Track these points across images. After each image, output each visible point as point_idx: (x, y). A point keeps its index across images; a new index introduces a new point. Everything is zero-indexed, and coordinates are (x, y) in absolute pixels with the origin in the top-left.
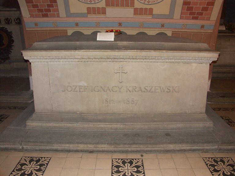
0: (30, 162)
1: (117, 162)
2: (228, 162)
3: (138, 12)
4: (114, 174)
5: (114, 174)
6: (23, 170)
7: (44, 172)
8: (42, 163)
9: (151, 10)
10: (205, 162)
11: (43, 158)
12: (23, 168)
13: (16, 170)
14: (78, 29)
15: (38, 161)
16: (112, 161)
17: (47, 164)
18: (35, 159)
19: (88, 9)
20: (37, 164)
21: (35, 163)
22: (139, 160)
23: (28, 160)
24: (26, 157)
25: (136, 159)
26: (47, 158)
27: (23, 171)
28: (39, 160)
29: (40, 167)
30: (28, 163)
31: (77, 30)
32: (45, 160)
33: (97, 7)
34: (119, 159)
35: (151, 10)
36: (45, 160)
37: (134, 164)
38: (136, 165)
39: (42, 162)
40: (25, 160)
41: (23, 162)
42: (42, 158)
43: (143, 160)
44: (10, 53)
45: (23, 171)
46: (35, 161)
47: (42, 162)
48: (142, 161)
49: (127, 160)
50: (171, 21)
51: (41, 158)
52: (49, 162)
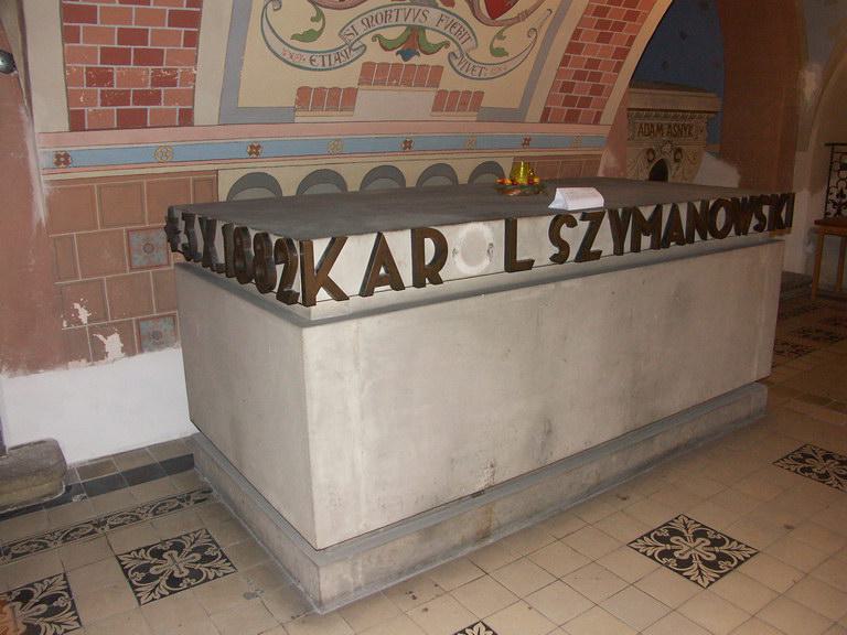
0: (697, 534)
1: (59, 624)
2: (159, 584)
3: (445, 102)
4: (65, 590)
5: (65, 590)
6: (672, 544)
7: (722, 575)
8: (659, 544)
9: (479, 95)
10: (228, 561)
11: (735, 543)
12: (673, 540)
13: (656, 536)
14: (259, 165)
15: (717, 542)
16: (120, 561)
17: (740, 562)
18: (710, 535)
19: (303, 92)
20: (674, 547)
21: (677, 554)
22: (150, 598)
23: (693, 528)
24: (696, 582)
25: (162, 596)
26: (747, 547)
27: (669, 547)
28: (721, 542)
29: (718, 559)
30: (689, 535)
31: (319, 168)
32: (648, 546)
33: (331, 87)
34: (216, 577)
35: (479, 95)
36: (648, 546)
37: (36, 596)
38: (157, 582)
39: (729, 550)
40: (685, 525)
41: (678, 526)
42: (731, 540)
43: (137, 603)
44: (817, 227)
45: (669, 547)
46: (710, 540)
47: (729, 550)
48: (636, 541)
49: (189, 586)
50: (517, 155)
51: (728, 541)
52: (746, 559)
